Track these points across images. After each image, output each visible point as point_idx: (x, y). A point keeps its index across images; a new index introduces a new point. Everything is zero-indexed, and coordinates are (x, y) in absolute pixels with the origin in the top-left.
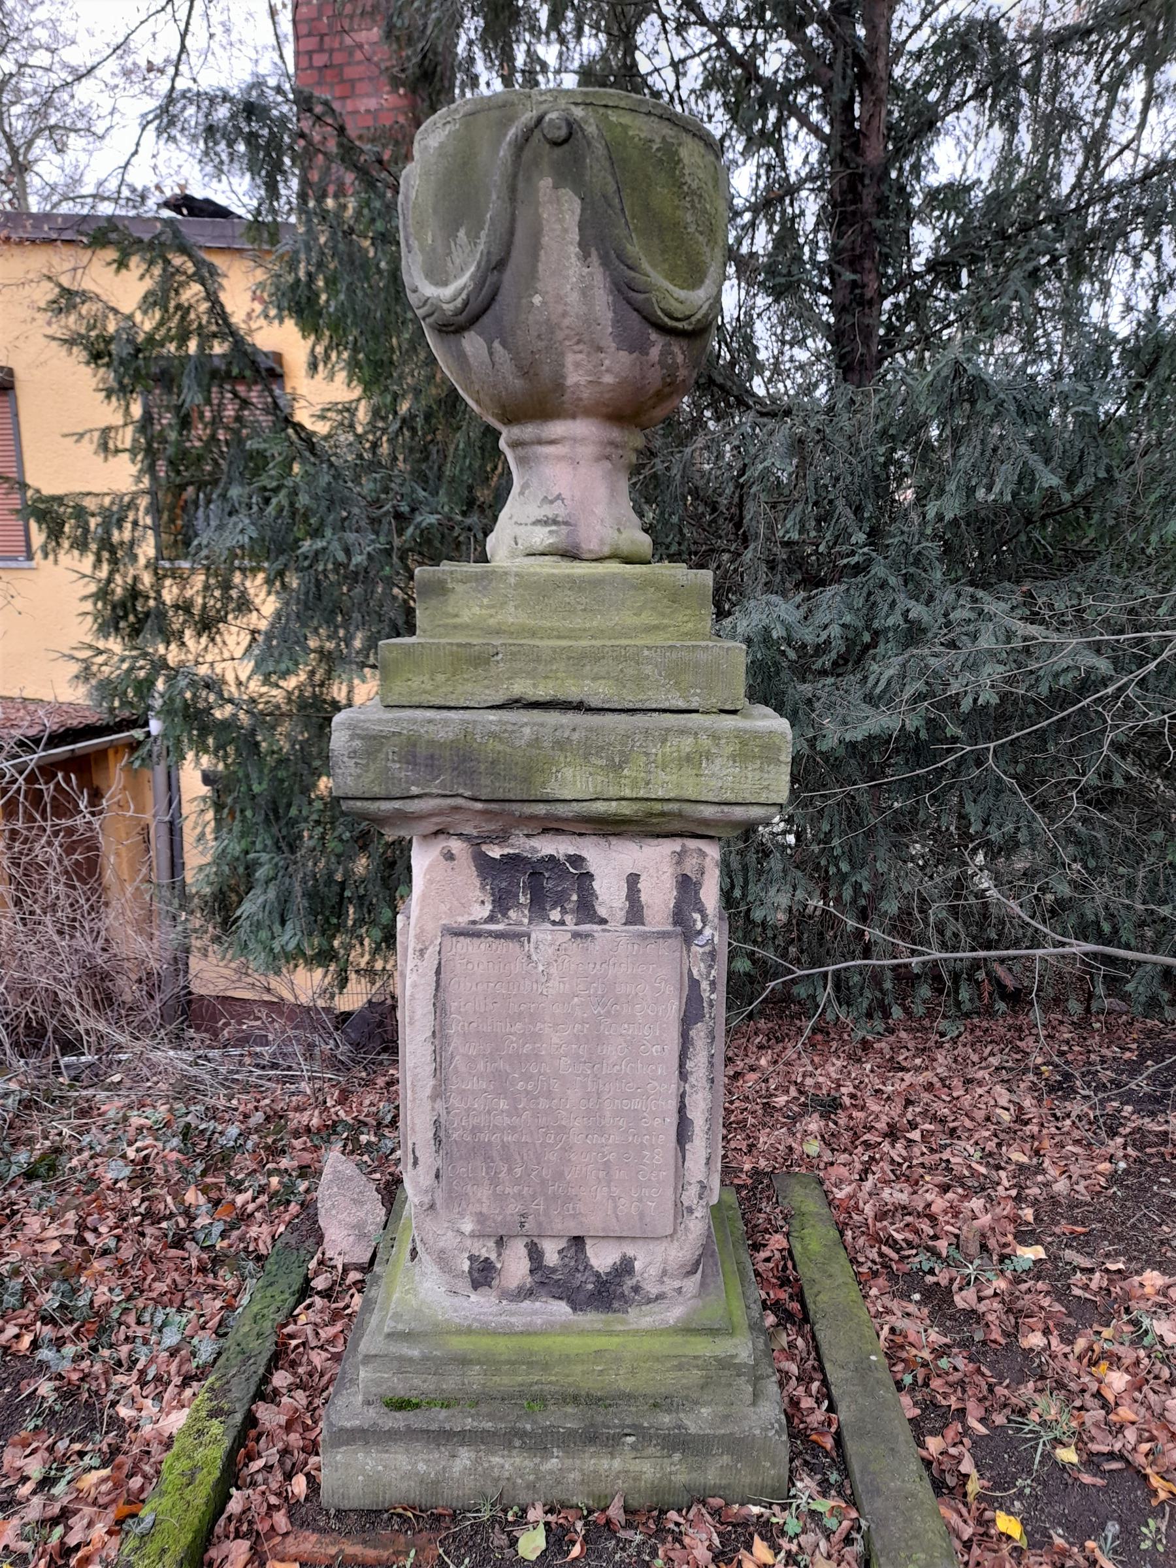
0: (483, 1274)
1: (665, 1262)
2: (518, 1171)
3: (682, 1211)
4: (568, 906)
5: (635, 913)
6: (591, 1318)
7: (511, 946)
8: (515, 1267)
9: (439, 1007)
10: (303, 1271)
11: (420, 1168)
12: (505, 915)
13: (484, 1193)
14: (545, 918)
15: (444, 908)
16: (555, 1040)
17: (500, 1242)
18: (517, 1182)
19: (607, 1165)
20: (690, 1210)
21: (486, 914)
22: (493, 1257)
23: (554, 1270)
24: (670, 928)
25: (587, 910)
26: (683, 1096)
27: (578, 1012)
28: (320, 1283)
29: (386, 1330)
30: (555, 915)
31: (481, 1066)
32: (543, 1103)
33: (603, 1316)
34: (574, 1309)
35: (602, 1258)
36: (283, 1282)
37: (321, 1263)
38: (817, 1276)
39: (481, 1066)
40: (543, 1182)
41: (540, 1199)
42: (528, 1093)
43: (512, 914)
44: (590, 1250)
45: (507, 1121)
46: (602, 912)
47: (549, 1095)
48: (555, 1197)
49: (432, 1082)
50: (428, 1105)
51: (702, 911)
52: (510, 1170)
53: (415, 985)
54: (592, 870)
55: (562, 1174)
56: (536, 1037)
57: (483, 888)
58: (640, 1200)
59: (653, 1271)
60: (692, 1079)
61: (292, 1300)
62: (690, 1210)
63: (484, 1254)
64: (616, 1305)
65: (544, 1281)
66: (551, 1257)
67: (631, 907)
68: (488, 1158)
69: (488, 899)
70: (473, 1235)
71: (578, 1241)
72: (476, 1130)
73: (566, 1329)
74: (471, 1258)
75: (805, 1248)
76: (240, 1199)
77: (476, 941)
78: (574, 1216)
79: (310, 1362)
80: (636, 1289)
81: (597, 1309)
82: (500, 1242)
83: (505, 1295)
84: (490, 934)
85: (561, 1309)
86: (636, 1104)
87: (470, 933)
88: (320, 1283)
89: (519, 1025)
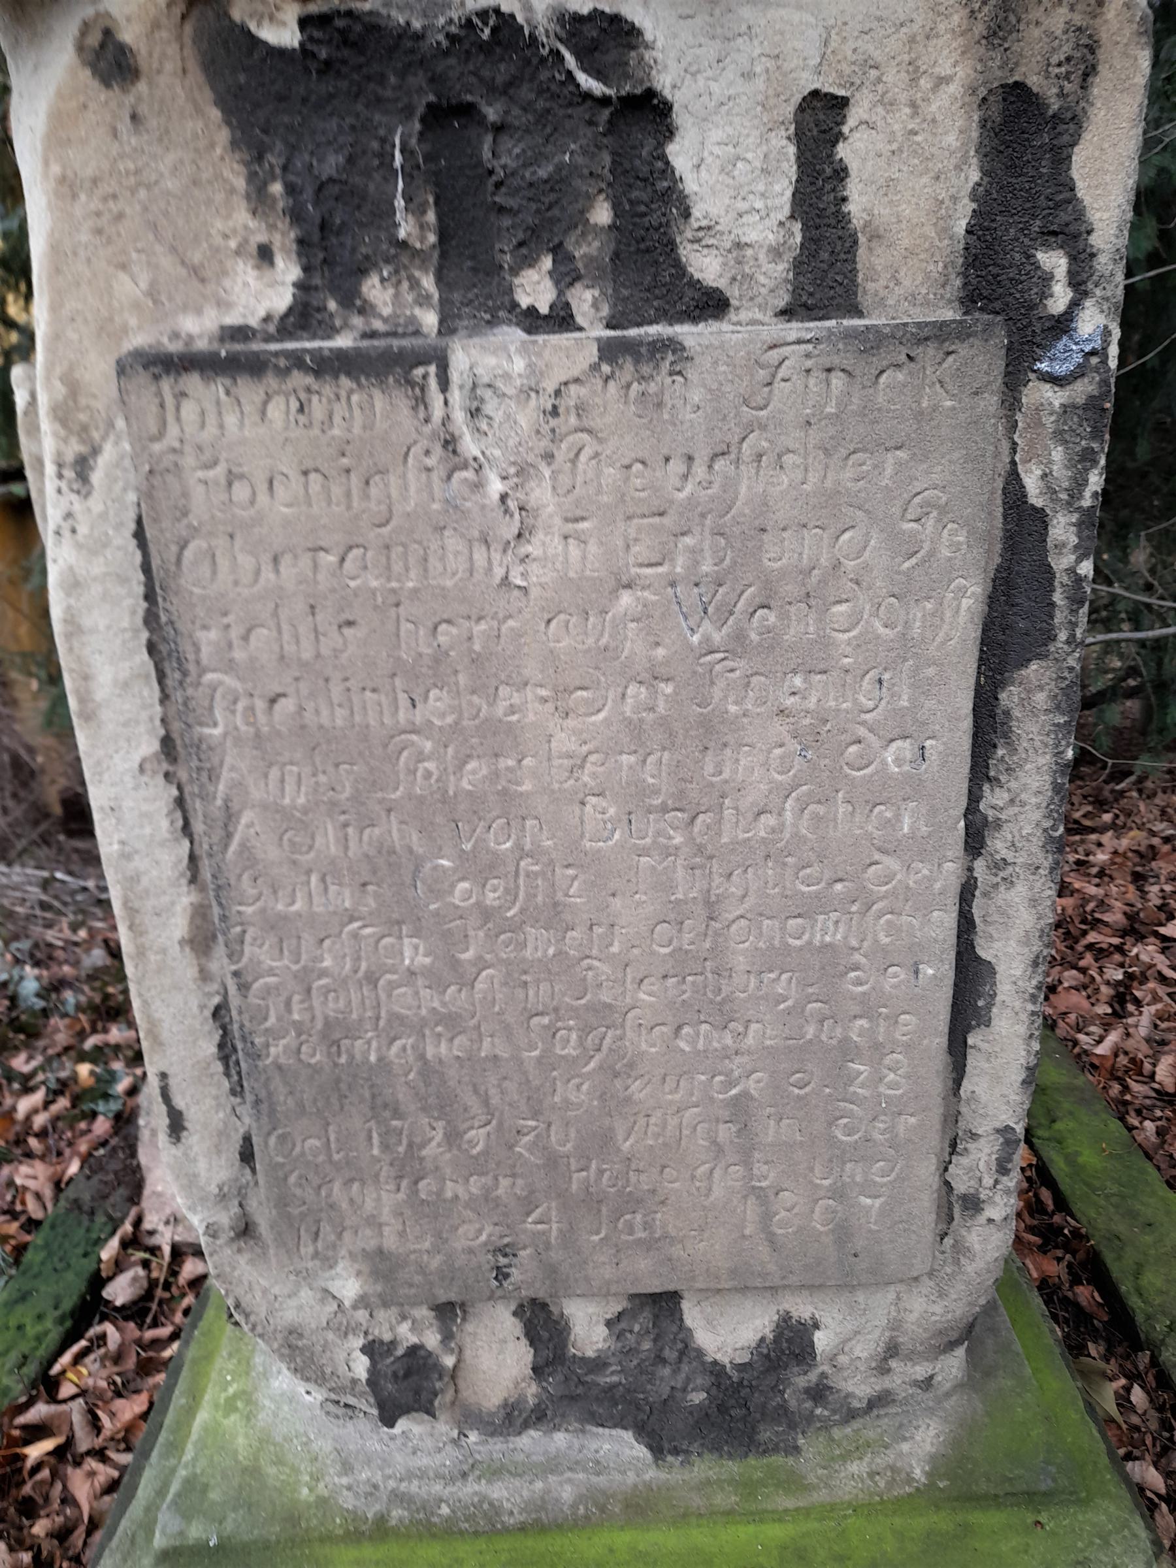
0: (405, 1385)
1: (896, 1325)
2: (478, 1137)
3: (954, 1206)
4: (584, 250)
5: (825, 267)
6: (701, 1473)
7: (381, 409)
8: (497, 1359)
9: (163, 651)
10: (88, 1266)
11: (194, 1139)
12: (351, 300)
13: (385, 1200)
14: (503, 309)
15: (128, 288)
16: (563, 742)
17: (448, 1313)
18: (476, 1166)
19: (740, 1110)
20: (973, 1204)
21: (281, 299)
22: (432, 1340)
23: (598, 1364)
24: (949, 314)
25: (654, 279)
26: (967, 892)
27: (633, 644)
28: (120, 1291)
29: (159, 1541)
30: (535, 288)
31: (328, 839)
32: (539, 944)
33: (733, 1467)
34: (658, 1451)
35: (725, 1333)
36: (46, 1289)
37: (131, 1243)
38: (1121, 1227)
39: (328, 839)
40: (552, 1161)
41: (548, 1207)
42: (486, 914)
43: (376, 290)
44: (692, 1314)
45: (430, 1000)
46: (706, 266)
47: (554, 915)
48: (592, 1200)
49: (186, 899)
50: (185, 966)
51: (1071, 235)
52: (453, 1137)
53: (74, 585)
54: (664, 82)
55: (606, 1140)
56: (499, 737)
57: (258, 198)
58: (839, 1193)
59: (864, 1349)
60: (998, 844)
61: (55, 1335)
62: (973, 1204)
63: (406, 1335)
64: (765, 1434)
65: (567, 1387)
66: (588, 1329)
67: (811, 245)
68: (383, 1108)
69: (283, 239)
70: (362, 1301)
71: (663, 1305)
72: (335, 1034)
73: (639, 1507)
74: (369, 1349)
75: (1071, 1160)
76: (24, 1105)
77: (249, 391)
78: (648, 1245)
79: (68, 1499)
80: (819, 1393)
81: (716, 1448)
82: (448, 1313)
83: (470, 1418)
84: (297, 361)
85: (620, 1451)
86: (829, 930)
87: (234, 359)
88: (120, 1291)
89: (438, 700)
